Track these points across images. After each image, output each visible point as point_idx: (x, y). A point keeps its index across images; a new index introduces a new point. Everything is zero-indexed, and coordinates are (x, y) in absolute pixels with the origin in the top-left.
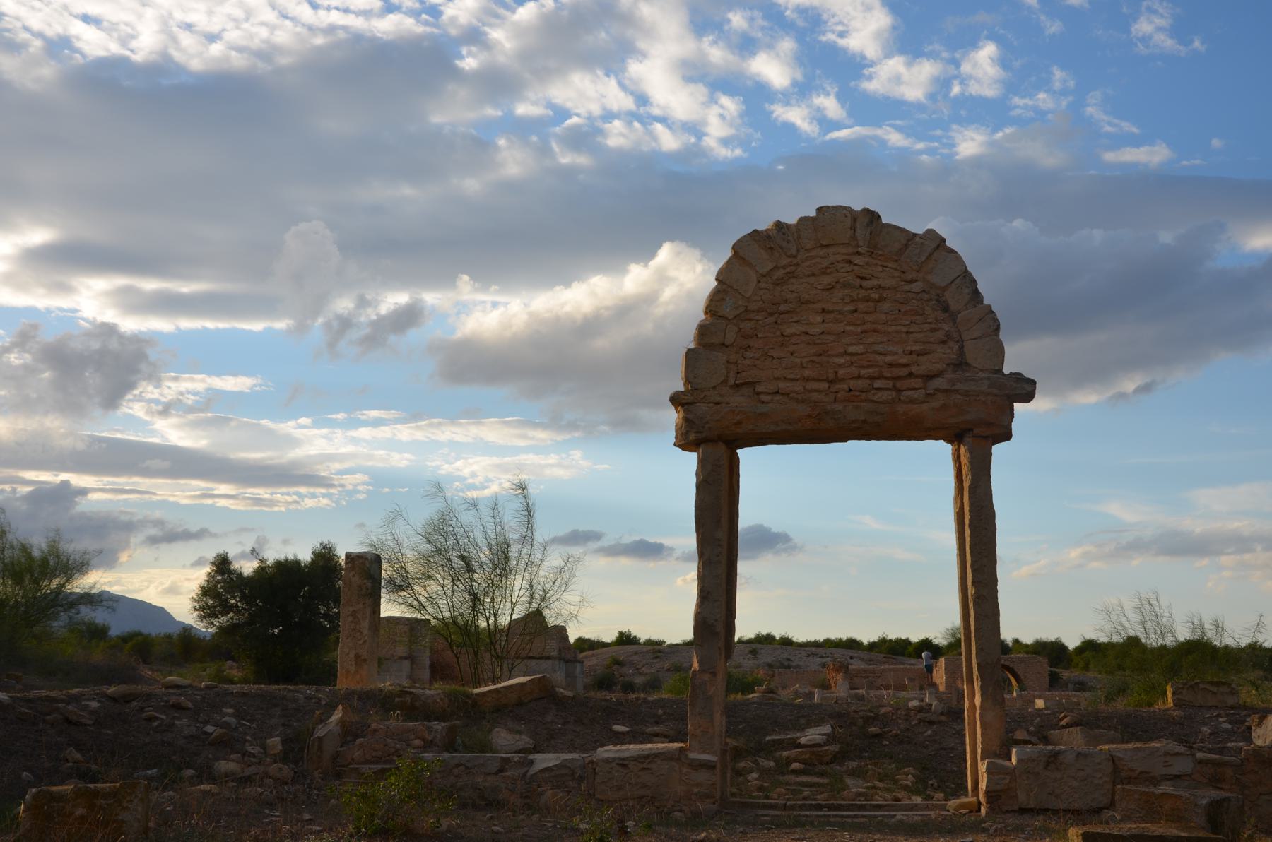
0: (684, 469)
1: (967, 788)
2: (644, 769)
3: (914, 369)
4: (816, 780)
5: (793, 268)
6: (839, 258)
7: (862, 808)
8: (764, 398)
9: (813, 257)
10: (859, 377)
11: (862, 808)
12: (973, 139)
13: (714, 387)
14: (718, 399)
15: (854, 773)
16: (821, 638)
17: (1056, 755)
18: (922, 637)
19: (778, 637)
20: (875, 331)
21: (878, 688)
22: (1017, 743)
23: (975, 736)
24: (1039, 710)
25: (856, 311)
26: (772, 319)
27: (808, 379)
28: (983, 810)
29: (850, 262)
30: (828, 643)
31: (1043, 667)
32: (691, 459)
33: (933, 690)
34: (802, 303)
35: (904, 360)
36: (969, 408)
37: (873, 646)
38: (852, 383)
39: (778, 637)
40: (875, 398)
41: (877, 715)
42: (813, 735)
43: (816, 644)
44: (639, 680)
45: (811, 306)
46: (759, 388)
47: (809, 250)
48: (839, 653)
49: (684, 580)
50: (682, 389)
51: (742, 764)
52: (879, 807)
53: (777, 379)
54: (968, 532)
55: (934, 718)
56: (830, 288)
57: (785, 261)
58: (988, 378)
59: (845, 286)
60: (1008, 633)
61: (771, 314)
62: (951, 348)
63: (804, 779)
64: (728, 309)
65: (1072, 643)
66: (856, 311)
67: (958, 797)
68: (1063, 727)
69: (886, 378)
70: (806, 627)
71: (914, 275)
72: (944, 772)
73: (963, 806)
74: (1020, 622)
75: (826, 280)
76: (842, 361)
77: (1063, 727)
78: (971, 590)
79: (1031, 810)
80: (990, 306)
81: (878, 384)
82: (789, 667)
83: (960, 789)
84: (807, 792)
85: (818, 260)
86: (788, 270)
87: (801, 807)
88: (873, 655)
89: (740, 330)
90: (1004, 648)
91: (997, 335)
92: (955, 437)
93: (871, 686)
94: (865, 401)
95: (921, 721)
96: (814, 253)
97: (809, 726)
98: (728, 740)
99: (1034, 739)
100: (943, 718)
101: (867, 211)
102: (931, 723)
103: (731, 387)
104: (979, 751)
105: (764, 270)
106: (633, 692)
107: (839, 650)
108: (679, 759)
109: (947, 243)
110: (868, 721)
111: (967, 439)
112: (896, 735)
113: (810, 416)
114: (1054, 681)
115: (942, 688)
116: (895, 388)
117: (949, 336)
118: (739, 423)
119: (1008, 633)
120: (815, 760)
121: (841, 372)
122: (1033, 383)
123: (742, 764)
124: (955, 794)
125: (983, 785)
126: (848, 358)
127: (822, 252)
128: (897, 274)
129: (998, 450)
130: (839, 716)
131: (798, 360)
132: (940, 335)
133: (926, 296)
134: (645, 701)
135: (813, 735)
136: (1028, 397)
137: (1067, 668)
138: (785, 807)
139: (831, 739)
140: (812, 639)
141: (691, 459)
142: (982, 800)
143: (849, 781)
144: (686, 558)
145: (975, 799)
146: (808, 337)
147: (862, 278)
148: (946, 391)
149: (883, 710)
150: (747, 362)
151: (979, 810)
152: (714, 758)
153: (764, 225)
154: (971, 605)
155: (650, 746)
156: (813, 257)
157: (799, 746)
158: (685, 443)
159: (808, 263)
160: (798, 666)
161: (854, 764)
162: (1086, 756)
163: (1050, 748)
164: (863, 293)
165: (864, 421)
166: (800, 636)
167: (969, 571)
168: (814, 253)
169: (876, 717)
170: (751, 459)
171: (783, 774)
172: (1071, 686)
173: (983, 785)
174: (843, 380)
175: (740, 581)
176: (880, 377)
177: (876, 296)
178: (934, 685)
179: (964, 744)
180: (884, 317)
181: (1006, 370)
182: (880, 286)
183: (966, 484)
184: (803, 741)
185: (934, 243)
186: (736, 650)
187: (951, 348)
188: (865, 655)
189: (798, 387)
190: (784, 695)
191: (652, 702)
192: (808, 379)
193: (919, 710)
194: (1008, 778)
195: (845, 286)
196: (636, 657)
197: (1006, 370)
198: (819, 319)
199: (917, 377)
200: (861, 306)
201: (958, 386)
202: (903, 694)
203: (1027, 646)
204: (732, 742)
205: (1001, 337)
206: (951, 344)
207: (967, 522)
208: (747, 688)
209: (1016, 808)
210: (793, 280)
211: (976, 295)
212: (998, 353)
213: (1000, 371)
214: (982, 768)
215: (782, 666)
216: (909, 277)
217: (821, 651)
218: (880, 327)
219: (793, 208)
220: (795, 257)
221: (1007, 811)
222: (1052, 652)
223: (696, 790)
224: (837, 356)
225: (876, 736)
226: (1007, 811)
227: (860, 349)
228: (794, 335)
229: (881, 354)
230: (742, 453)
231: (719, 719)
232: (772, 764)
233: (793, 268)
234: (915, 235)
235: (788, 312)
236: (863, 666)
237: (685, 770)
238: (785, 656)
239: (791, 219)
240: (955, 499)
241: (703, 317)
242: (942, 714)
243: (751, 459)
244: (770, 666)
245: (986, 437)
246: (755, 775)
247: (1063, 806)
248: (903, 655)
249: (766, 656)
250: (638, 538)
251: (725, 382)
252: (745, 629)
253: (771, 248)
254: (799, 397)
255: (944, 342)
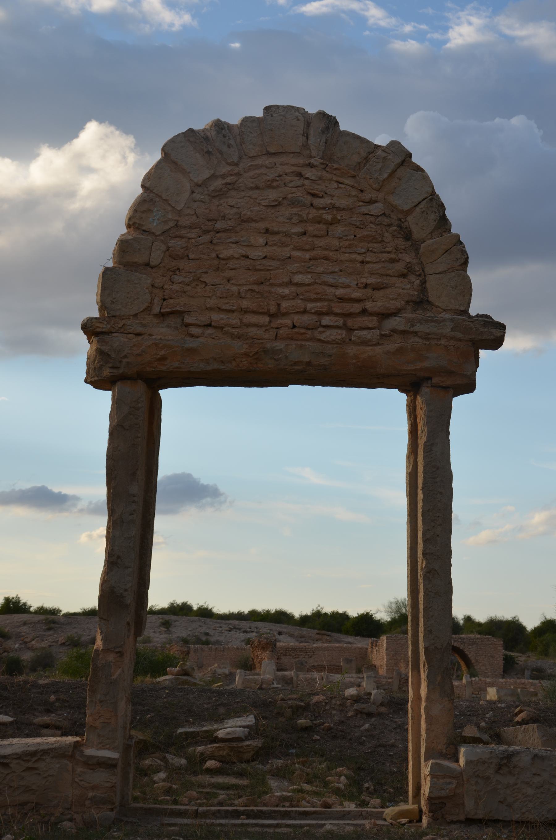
0: (89, 415)
1: (407, 793)
2: (29, 769)
3: (369, 305)
4: (233, 781)
5: (234, 178)
6: (288, 169)
7: (286, 815)
8: (194, 331)
9: (258, 167)
10: (305, 312)
11: (286, 815)
12: (470, 23)
13: (135, 315)
14: (140, 329)
15: (278, 774)
16: (246, 609)
17: (509, 757)
18: (362, 611)
19: (195, 608)
20: (326, 258)
21: (309, 671)
22: (466, 741)
23: (420, 730)
24: (491, 702)
25: (304, 234)
26: (206, 238)
27: (246, 311)
28: (425, 820)
29: (300, 175)
30: (254, 616)
31: (497, 649)
32: (104, 399)
33: (371, 673)
34: (244, 221)
35: (356, 295)
36: (429, 355)
37: (305, 620)
38: (296, 317)
39: (195, 608)
40: (322, 337)
41: (308, 704)
42: (233, 727)
43: (240, 616)
44: (27, 656)
45: (253, 225)
46: (189, 319)
47: (253, 158)
48: (265, 627)
49: (90, 537)
50: (96, 314)
51: (148, 762)
52: (305, 815)
53: (210, 309)
54: (420, 496)
55: (373, 709)
56: (276, 205)
57: (224, 169)
58: (452, 320)
59: (294, 203)
60: (459, 611)
61: (206, 232)
62: (412, 283)
63: (220, 780)
64: (154, 223)
65: (531, 623)
66: (304, 234)
67: (397, 803)
68: (518, 723)
69: (337, 315)
70: (227, 599)
71: (373, 195)
72: (381, 775)
73: (402, 814)
74: (474, 598)
75: (272, 195)
76: (286, 291)
77: (518, 723)
78: (421, 562)
79: (480, 821)
80: (458, 236)
81: (326, 321)
82: (207, 643)
83: (399, 794)
84: (222, 795)
85: (263, 170)
86: (229, 180)
87: (215, 814)
88: (305, 631)
89: (168, 248)
90: (456, 628)
91: (465, 270)
92: (410, 386)
93: (301, 667)
94: (311, 339)
95: (358, 712)
96: (259, 162)
97: (228, 716)
98: (133, 732)
99: (485, 737)
100: (383, 709)
101: (322, 115)
102: (369, 715)
103: (156, 315)
104: (423, 750)
105: (199, 179)
106: (21, 673)
107: (267, 624)
108: (72, 756)
109: (414, 159)
110: (298, 711)
111: (425, 390)
112: (330, 729)
113: (246, 355)
114: (509, 666)
115: (382, 671)
116: (345, 327)
117: (409, 268)
118: (163, 359)
119: (459, 611)
120: (234, 755)
121: (285, 305)
122: (502, 327)
123: (148, 762)
124: (393, 800)
125: (426, 790)
126: (293, 289)
127: (268, 161)
128: (354, 193)
129: (460, 404)
130: (262, 704)
131: (234, 289)
132: (400, 267)
133: (386, 221)
134: (35, 685)
135: (233, 727)
136: (496, 343)
137: (523, 653)
138: (196, 814)
139: (253, 732)
140: (235, 609)
141: (104, 399)
142: (424, 808)
143: (273, 783)
144: (94, 510)
145: (415, 806)
146: (248, 262)
147: (314, 195)
148: (403, 332)
149: (315, 699)
150: (176, 287)
151: (420, 820)
152: (115, 755)
153: (200, 123)
154: (421, 580)
155: (38, 740)
156: (258, 167)
157: (216, 740)
158: (97, 379)
159: (251, 174)
160: (218, 642)
161: (278, 763)
162: (543, 758)
163: (502, 748)
164: (313, 213)
165: (309, 364)
166: (222, 606)
167: (420, 541)
168: (259, 162)
169: (306, 708)
170: (175, 402)
171: (195, 773)
172: (527, 673)
173: (426, 790)
174: (285, 314)
175: (156, 539)
176: (329, 313)
177: (328, 217)
178: (373, 668)
179: (406, 740)
180: (336, 243)
181: (473, 312)
182: (333, 206)
183: (422, 441)
184: (221, 734)
185: (399, 158)
186: (150, 619)
187: (412, 283)
188: (297, 631)
189: (234, 320)
190: (199, 676)
191: (43, 686)
192: (246, 311)
193: (357, 699)
194: (455, 782)
195: (294, 203)
196: (25, 629)
197: (473, 312)
198: (261, 241)
199: (371, 314)
200: (311, 228)
201: (418, 328)
202: (337, 677)
203: (479, 624)
204: (138, 735)
205: (469, 273)
206: (412, 278)
207: (420, 485)
208: (158, 667)
209: (462, 818)
210: (233, 193)
211: (443, 222)
212: (465, 289)
213: (466, 312)
214: (426, 770)
215: (198, 641)
216: (367, 196)
217: (245, 624)
218: (331, 254)
219: (240, 104)
220: (237, 164)
221: (452, 822)
222: (507, 632)
223: (90, 794)
224: (280, 285)
225: (306, 729)
226: (452, 822)
227: (306, 278)
228: (232, 257)
229: (331, 286)
230: (164, 393)
231: (124, 707)
232: (183, 761)
233: (234, 178)
234: (377, 147)
235: (225, 231)
236: (293, 643)
237: (79, 770)
238: (204, 629)
239: (234, 119)
240: (408, 458)
241: (124, 230)
242: (382, 704)
243: (175, 402)
244: (185, 641)
245: (446, 388)
246: (162, 775)
247: (516, 817)
248: (339, 631)
249: (182, 628)
250: (39, 485)
251: (148, 309)
252: (158, 597)
253: (208, 152)
254: (235, 331)
255: (404, 276)
